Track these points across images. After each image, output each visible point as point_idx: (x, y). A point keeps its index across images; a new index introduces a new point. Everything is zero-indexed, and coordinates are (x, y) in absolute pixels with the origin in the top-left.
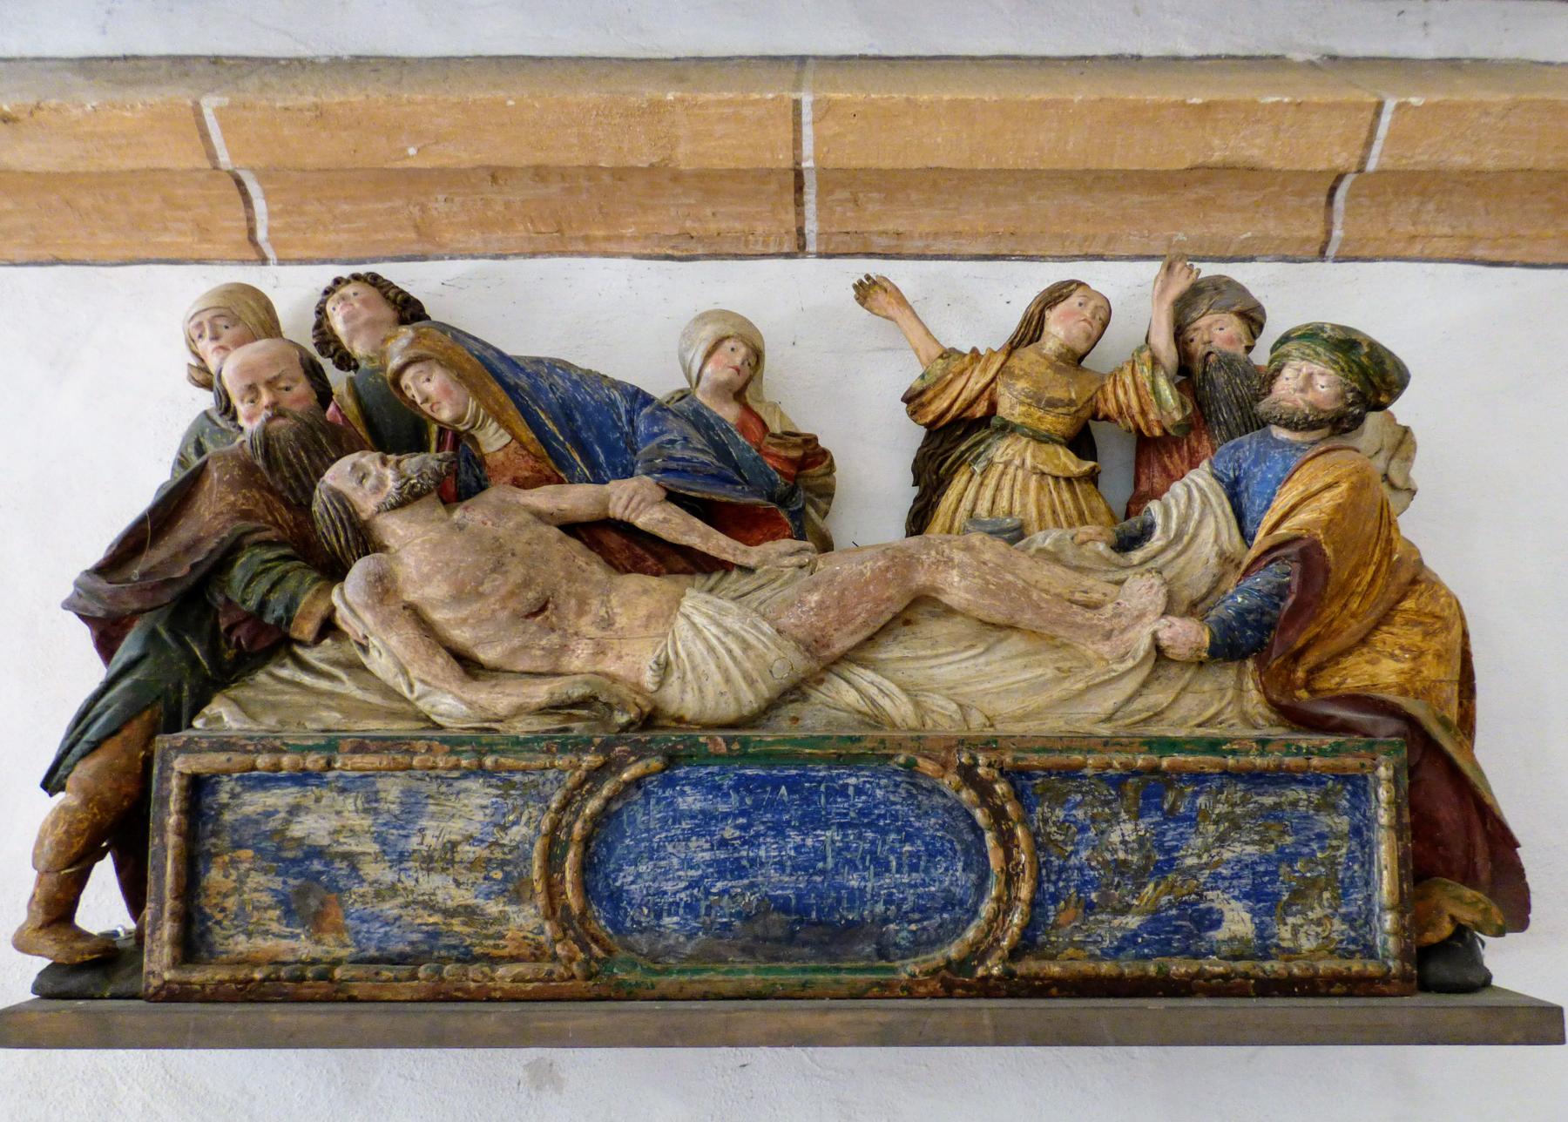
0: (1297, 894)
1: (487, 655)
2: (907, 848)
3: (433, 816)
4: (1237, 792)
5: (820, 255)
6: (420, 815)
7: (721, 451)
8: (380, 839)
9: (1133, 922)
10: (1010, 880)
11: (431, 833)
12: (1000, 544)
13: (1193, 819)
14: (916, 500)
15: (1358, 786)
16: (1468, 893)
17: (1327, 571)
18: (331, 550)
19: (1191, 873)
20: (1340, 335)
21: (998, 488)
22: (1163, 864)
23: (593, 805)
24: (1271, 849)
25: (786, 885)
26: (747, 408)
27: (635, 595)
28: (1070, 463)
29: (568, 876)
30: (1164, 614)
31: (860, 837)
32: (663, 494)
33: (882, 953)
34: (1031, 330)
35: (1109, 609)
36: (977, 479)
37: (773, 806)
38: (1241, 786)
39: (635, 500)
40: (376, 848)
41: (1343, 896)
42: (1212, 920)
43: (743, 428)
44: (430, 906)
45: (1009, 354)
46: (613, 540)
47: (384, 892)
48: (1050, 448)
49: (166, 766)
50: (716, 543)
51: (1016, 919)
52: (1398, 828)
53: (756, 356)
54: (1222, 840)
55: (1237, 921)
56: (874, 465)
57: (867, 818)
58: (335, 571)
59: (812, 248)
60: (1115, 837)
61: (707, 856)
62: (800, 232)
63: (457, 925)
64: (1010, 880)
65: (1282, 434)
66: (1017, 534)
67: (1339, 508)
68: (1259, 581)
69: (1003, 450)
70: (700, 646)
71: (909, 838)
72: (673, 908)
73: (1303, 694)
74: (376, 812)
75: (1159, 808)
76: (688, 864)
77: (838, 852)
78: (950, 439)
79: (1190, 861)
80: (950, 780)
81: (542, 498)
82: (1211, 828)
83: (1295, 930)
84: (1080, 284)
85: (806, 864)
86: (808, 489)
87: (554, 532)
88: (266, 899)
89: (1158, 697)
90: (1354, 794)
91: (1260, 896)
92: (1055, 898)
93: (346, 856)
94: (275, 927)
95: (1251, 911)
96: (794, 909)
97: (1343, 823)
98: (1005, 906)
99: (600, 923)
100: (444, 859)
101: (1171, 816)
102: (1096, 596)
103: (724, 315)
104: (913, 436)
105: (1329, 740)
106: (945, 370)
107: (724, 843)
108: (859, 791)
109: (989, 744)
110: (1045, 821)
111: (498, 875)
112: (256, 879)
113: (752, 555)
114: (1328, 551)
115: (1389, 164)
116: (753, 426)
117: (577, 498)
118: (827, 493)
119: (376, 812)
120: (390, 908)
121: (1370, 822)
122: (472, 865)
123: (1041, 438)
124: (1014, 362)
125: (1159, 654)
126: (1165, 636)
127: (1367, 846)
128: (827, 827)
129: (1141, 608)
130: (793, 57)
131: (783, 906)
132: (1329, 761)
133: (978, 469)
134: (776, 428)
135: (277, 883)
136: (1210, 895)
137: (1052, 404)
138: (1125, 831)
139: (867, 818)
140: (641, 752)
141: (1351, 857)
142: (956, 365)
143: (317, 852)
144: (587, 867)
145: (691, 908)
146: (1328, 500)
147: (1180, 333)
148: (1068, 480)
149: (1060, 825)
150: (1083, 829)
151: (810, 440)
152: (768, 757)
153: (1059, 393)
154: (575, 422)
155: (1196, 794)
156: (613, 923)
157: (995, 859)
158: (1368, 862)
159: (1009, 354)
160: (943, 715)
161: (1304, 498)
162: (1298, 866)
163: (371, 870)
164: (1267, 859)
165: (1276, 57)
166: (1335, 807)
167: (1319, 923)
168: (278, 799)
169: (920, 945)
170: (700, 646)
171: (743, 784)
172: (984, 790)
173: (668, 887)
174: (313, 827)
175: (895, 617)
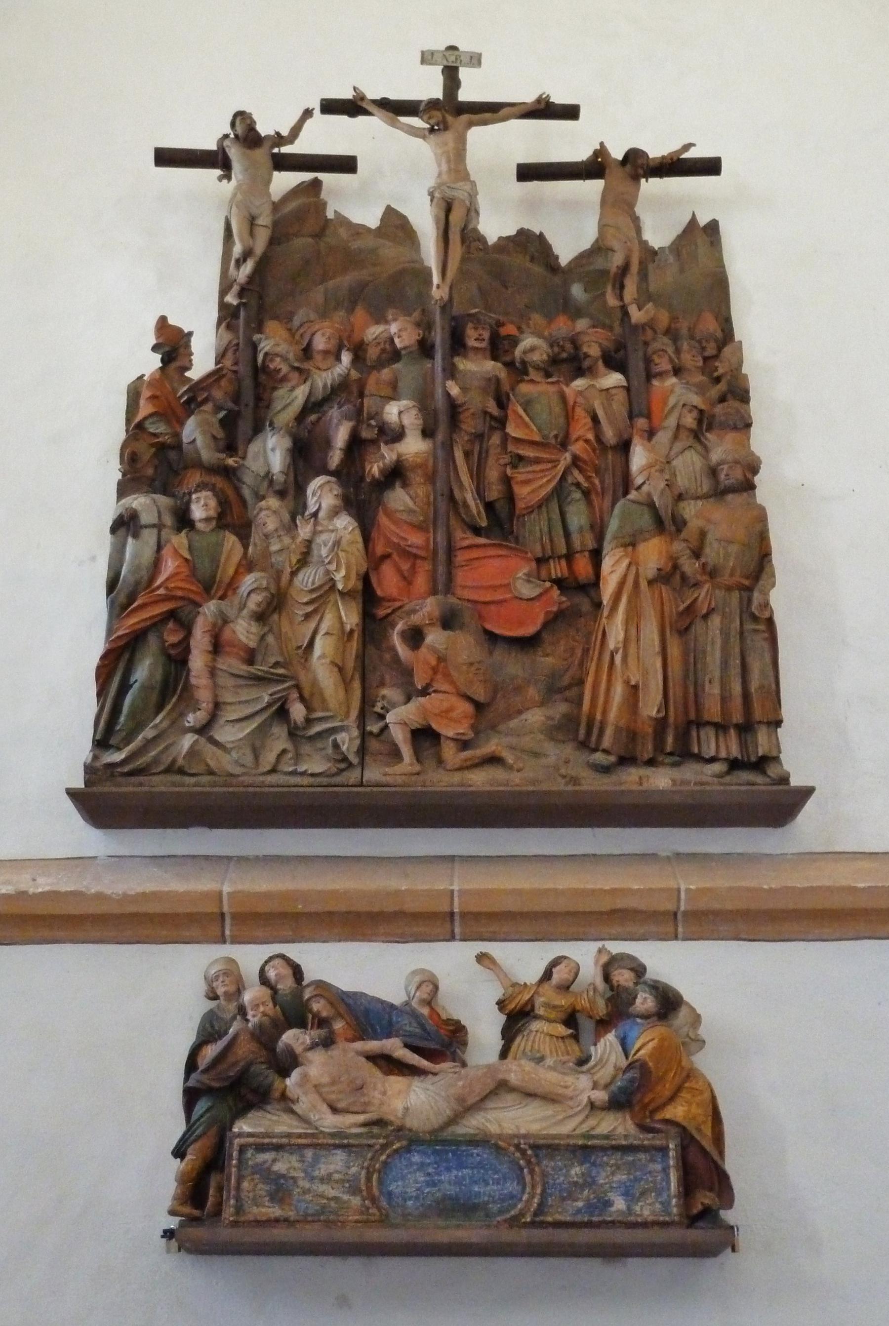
0: (643, 1194)
1: (341, 1105)
2: (496, 1176)
3: (324, 1163)
4: (619, 1155)
5: (461, 940)
6: (318, 1163)
7: (423, 1028)
8: (305, 1171)
9: (580, 1204)
10: (533, 1187)
11: (323, 1169)
12: (533, 1064)
13: (603, 1165)
14: (503, 1046)
15: (664, 1150)
16: (708, 1194)
17: (650, 1072)
18: (285, 1064)
19: (602, 1185)
20: (652, 983)
21: (534, 1041)
22: (589, 1182)
23: (383, 1157)
24: (632, 1177)
25: (451, 1190)
26: (432, 1009)
27: (396, 1082)
28: (562, 1030)
29: (374, 1184)
30: (593, 1089)
31: (479, 1172)
32: (402, 1045)
33: (487, 1216)
34: (547, 975)
35: (571, 1089)
36: (525, 1038)
37: (447, 1160)
38: (620, 1153)
39: (395, 1047)
40: (302, 1175)
41: (659, 1195)
42: (608, 1203)
43: (431, 1016)
44: (322, 1196)
45: (539, 986)
46: (383, 1063)
47: (306, 1192)
48: (554, 1024)
49: (231, 1144)
50: (424, 1063)
51: (536, 1200)
52: (677, 1167)
53: (436, 988)
54: (613, 1174)
55: (620, 1204)
56: (485, 1030)
57: (480, 1165)
58: (285, 1073)
59: (457, 937)
60: (573, 1172)
61: (422, 1179)
62: (453, 932)
63: (333, 1204)
64: (533, 1187)
65: (639, 1020)
66: (540, 1060)
67: (654, 1048)
68: (628, 1075)
69: (535, 1025)
70: (416, 1100)
71: (496, 1173)
72: (410, 1198)
73: (648, 1120)
74: (303, 1161)
75: (589, 1162)
76: (416, 1182)
77: (471, 1178)
78: (517, 1017)
79: (602, 1181)
80: (512, 1149)
81: (359, 1045)
82: (609, 1169)
83: (642, 1207)
84: (565, 958)
85: (459, 1182)
86: (457, 1042)
87: (364, 1060)
88: (264, 1193)
89: (592, 1122)
90: (663, 1156)
91: (627, 1194)
92: (551, 1195)
93: (293, 1178)
94: (267, 1204)
95: (625, 1200)
96: (454, 1199)
97: (658, 1167)
98: (532, 1196)
99: (384, 1203)
100: (326, 1179)
101: (594, 1164)
102: (570, 1084)
103: (423, 971)
104: (502, 1018)
105: (651, 1135)
106: (513, 992)
107: (429, 1174)
108: (478, 1155)
109: (525, 1136)
110: (547, 1166)
111: (347, 1185)
112: (260, 1186)
113: (437, 1067)
114: (651, 1064)
115: (689, 908)
116: (435, 1016)
117: (373, 1045)
118: (465, 1044)
119: (303, 1161)
120: (308, 1197)
121: (668, 1167)
122: (337, 1182)
123: (549, 1020)
124: (540, 989)
125: (592, 1105)
126: (593, 1097)
127: (668, 1175)
128: (466, 1168)
129: (583, 1087)
130: (449, 856)
131: (450, 1198)
132: (650, 1142)
133: (525, 1033)
134: (444, 1017)
135: (267, 1188)
136: (609, 1194)
137: (555, 1007)
138: (576, 1171)
139: (480, 1165)
140: (399, 1139)
141: (662, 1180)
142: (517, 989)
143: (283, 1176)
144: (381, 1182)
145: (417, 1198)
146: (651, 1045)
147: (607, 978)
148: (562, 1038)
149: (553, 1169)
150: (561, 1170)
151: (458, 1022)
152: (444, 1142)
153: (557, 1003)
154: (365, 1017)
155: (603, 1156)
156: (389, 1204)
157: (528, 1178)
158: (668, 1183)
159: (539, 986)
160: (509, 1128)
161: (646, 1041)
162: (642, 1183)
163: (301, 1183)
164: (630, 1180)
165: (653, 854)
166: (655, 1161)
167: (650, 1204)
168: (268, 1156)
169: (501, 1212)
170: (416, 1100)
171: (435, 1152)
172: (523, 1153)
173: (409, 1190)
174: (280, 1167)
175: (491, 1092)
